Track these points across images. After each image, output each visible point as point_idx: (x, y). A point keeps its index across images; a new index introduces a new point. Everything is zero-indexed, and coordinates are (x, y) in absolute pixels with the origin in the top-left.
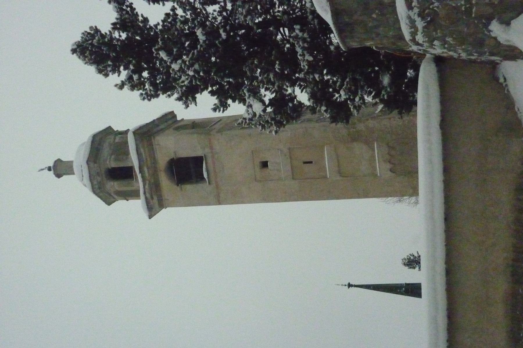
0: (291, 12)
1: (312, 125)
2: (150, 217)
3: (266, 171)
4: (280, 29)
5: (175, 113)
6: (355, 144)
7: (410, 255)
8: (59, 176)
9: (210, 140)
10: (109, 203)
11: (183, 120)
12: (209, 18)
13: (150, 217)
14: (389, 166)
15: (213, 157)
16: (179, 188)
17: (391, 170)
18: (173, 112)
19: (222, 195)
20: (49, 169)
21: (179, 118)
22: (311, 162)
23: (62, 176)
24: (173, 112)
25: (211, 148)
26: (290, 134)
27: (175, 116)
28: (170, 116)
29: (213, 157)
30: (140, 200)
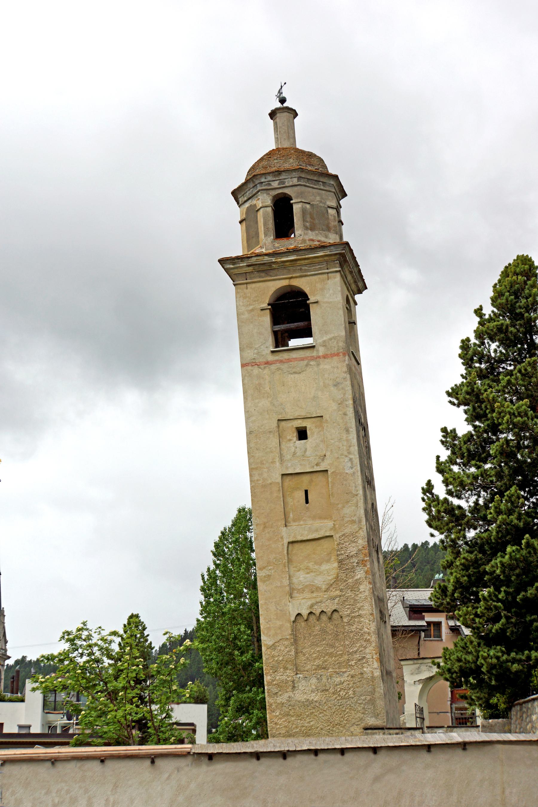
0: (503, 464)
1: (361, 504)
2: (222, 261)
3: (294, 435)
4: (508, 545)
5: (365, 292)
6: (336, 565)
7: (43, 656)
8: (273, 115)
9: (338, 355)
10: (433, 486)
11: (356, 304)
12: (522, 544)
13: (222, 261)
14: (305, 613)
15: (313, 358)
16: (265, 305)
17: (299, 615)
18: (366, 288)
19: (256, 371)
20: (283, 101)
21: (357, 297)
22: (307, 502)
23: (272, 118)
24: (366, 288)
25: (325, 357)
26: (347, 472)
27: (360, 292)
28: (360, 284)
29: (313, 358)
30: (312, 338)
